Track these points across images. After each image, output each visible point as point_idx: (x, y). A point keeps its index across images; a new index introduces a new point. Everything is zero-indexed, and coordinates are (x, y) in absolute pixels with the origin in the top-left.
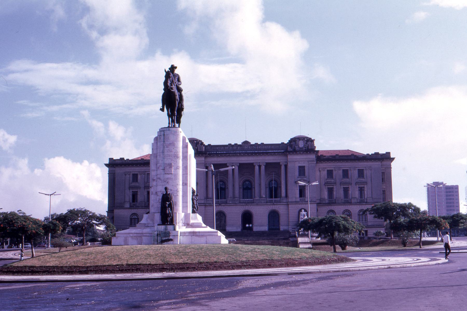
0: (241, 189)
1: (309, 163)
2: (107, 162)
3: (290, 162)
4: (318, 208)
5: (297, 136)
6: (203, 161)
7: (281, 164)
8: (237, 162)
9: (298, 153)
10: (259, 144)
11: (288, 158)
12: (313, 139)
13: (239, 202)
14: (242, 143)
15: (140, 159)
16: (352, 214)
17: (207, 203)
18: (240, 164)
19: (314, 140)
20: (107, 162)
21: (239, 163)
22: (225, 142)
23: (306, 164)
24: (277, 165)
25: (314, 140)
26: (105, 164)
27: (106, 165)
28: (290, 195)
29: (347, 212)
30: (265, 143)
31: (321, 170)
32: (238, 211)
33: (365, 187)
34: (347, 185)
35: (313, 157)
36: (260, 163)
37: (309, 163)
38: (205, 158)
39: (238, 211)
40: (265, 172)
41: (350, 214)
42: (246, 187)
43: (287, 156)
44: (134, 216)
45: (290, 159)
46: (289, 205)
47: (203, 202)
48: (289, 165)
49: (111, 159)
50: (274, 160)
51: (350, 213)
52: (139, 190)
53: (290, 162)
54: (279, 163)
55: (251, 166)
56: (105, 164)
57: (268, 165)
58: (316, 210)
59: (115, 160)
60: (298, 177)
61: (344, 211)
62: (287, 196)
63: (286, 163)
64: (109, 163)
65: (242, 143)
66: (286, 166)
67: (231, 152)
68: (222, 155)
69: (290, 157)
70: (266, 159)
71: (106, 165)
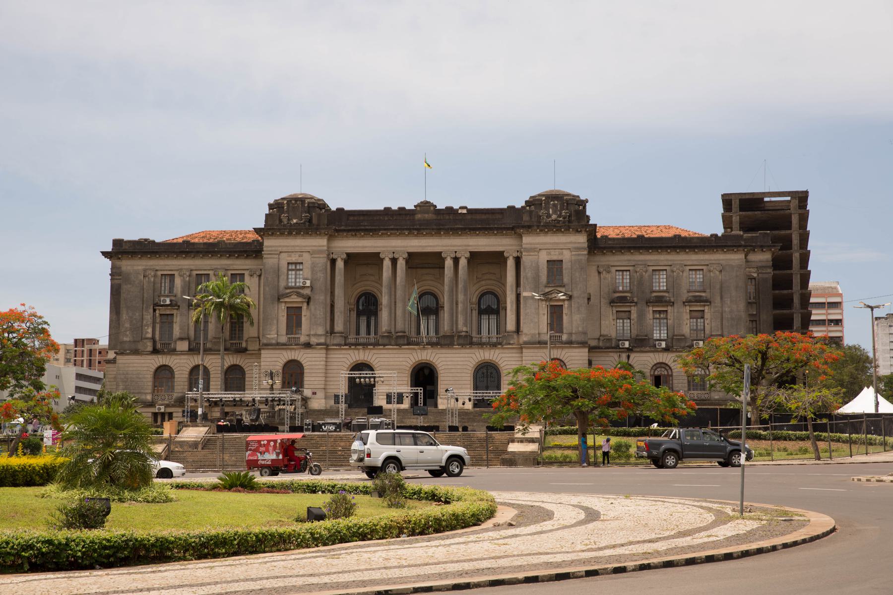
0: (474, 312)
1: (573, 253)
2: (109, 248)
3: (528, 250)
4: (593, 359)
5: (546, 192)
6: (323, 246)
7: (382, 256)
8: (402, 249)
9: (442, 233)
10: (395, 211)
11: (523, 242)
12: (583, 198)
13: (406, 342)
14: (415, 206)
15: (180, 241)
16: (674, 374)
17: (332, 343)
18: (348, 255)
19: (587, 201)
20: (109, 248)
21: (346, 253)
22: (377, 205)
23: (566, 256)
24: (498, 258)
25: (587, 201)
26: (102, 252)
27: (105, 254)
28: (524, 327)
29: (663, 369)
30: (346, 209)
31: (601, 270)
32: (404, 363)
33: (706, 311)
34: (701, 306)
35: (581, 239)
36: (456, 252)
37: (573, 253)
38: (329, 240)
39: (404, 363)
40: (406, 277)
41: (670, 373)
42: (485, 307)
43: (521, 237)
44: (658, 370)
45: (527, 244)
46: (524, 350)
47: (322, 340)
48: (526, 260)
49: (117, 243)
50: (489, 246)
51: (669, 371)
52: (633, 308)
53: (528, 250)
54: (502, 253)
55: (434, 261)
56: (102, 252)
57: (475, 258)
58: (587, 362)
59: (159, 244)
60: (546, 287)
61: (655, 365)
62: (518, 330)
63: (519, 254)
64: (112, 249)
65: (415, 206)
66: (518, 261)
67: (367, 227)
68: (422, 233)
69: (528, 240)
70: (471, 244)
71: (105, 254)
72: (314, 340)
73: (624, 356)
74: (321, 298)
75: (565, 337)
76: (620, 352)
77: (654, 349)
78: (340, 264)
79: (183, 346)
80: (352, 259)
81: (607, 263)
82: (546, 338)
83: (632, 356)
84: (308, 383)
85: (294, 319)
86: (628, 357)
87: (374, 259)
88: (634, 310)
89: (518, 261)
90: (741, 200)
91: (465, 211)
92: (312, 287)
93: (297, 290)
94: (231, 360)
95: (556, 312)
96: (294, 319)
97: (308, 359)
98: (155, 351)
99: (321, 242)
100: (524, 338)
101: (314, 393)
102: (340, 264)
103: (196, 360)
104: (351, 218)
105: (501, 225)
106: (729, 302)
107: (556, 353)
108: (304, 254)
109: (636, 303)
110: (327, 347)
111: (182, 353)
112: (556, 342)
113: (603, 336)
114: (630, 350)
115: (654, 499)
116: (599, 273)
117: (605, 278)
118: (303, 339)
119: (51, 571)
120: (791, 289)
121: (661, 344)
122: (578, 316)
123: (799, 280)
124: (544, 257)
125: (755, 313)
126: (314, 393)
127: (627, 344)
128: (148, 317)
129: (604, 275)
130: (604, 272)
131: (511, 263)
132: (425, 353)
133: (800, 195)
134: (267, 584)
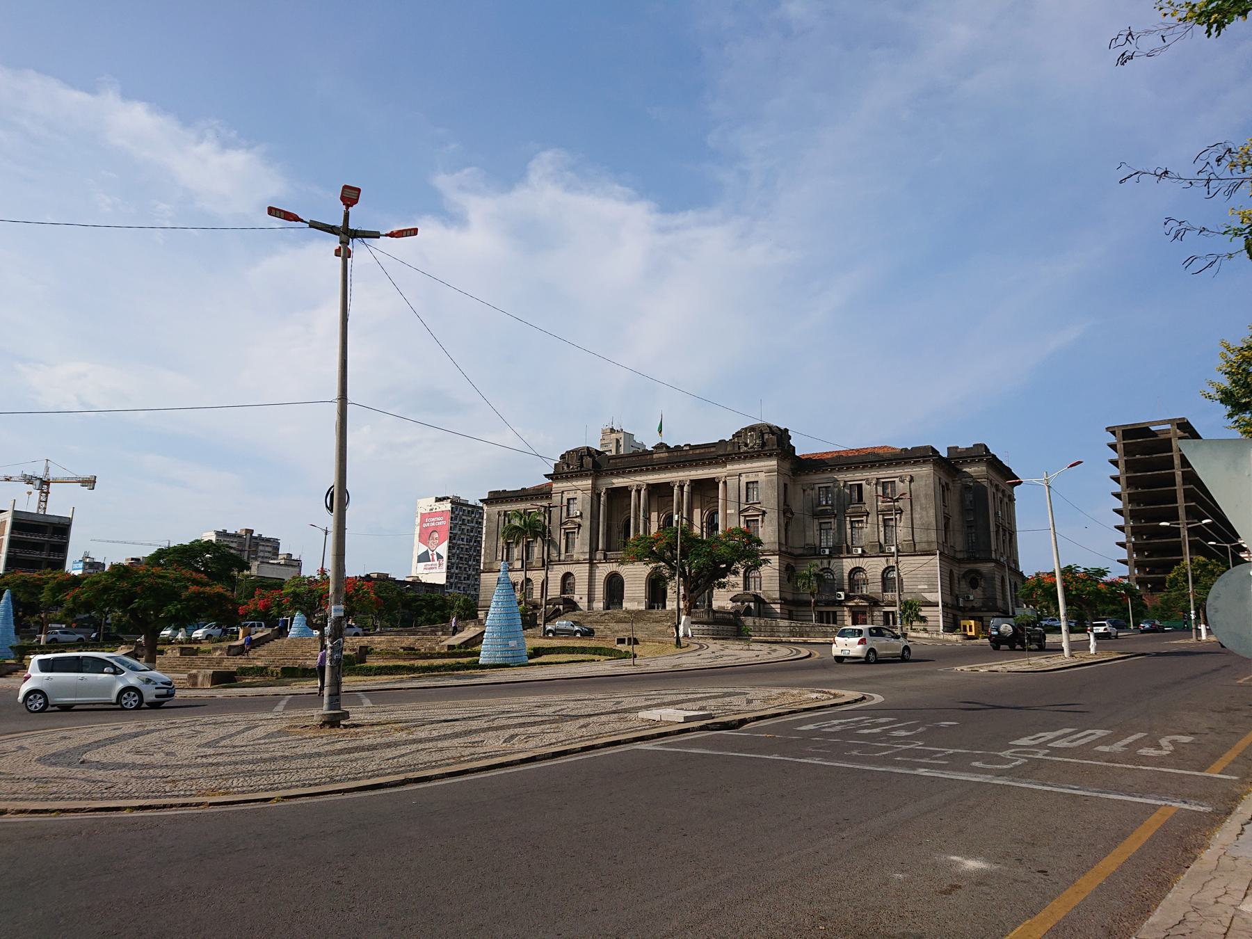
23: (762, 477)
66: (725, 483)
73: (825, 561)
74: (586, 523)
76: (821, 558)
81: (810, 482)
83: (833, 561)
84: (642, 591)
86: (829, 563)
87: (625, 491)
90: (1123, 431)
91: (688, 448)
101: (581, 598)
104: (611, 461)
106: (919, 510)
108: (578, 491)
109: (836, 515)
113: (807, 545)
115: (674, 698)
116: (804, 491)
117: (809, 495)
120: (1177, 503)
121: (857, 550)
122: (771, 528)
123: (1183, 495)
125: (972, 519)
126: (581, 598)
127: (827, 552)
129: (809, 491)
130: (808, 490)
131: (721, 485)
132: (947, 575)
133: (1178, 422)
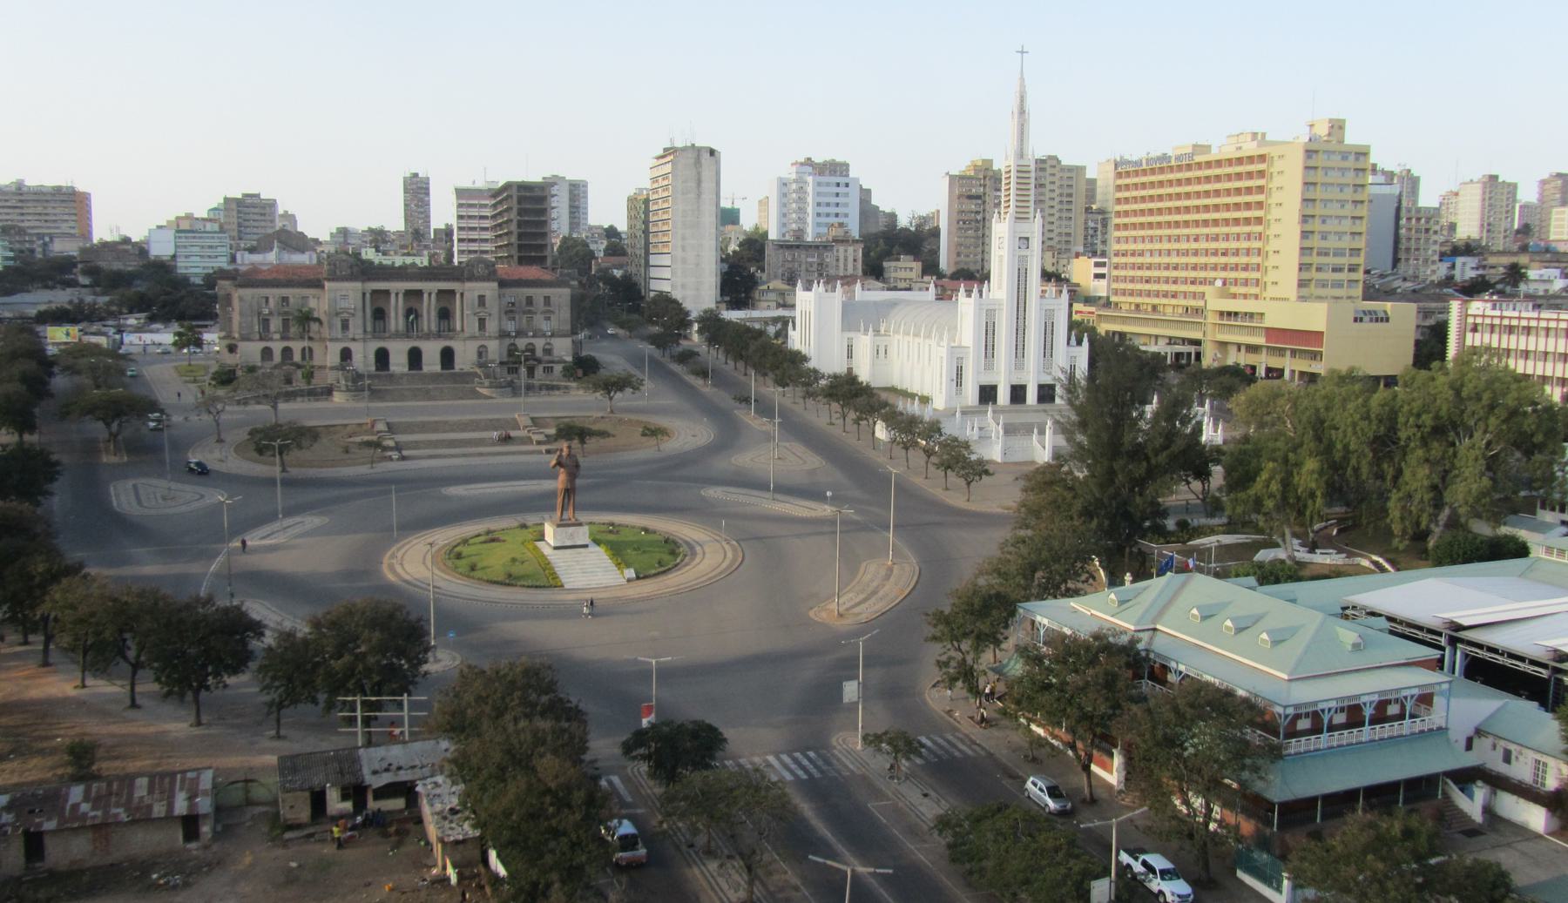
24: (452, 292)
57: (440, 292)
62: (463, 330)
66: (462, 295)
69: (468, 285)
72: (357, 337)
74: (360, 314)
75: (487, 334)
77: (527, 336)
78: (368, 296)
79: (277, 336)
80: (374, 292)
82: (477, 334)
85: (345, 326)
87: (387, 293)
88: (517, 317)
89: (462, 295)
92: (355, 309)
93: (345, 310)
94: (306, 343)
95: (482, 322)
96: (345, 326)
97: (353, 346)
98: (261, 339)
99: (358, 285)
100: (466, 335)
102: (368, 296)
103: (286, 344)
105: (868, 586)
107: (483, 343)
110: (364, 340)
111: (276, 340)
112: (482, 337)
114: (516, 337)
118: (351, 336)
119: (587, 510)
124: (476, 294)
128: (256, 320)
131: (458, 296)
134: (1502, 660)
